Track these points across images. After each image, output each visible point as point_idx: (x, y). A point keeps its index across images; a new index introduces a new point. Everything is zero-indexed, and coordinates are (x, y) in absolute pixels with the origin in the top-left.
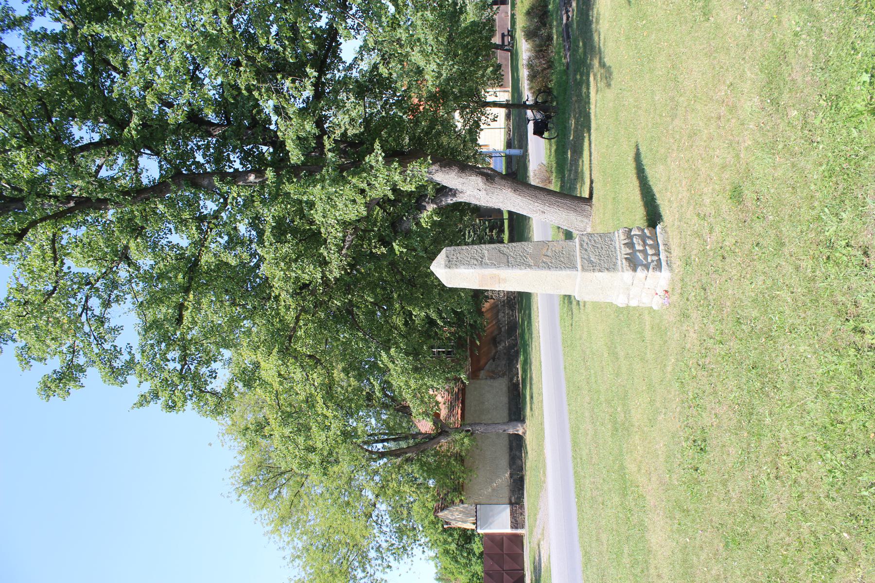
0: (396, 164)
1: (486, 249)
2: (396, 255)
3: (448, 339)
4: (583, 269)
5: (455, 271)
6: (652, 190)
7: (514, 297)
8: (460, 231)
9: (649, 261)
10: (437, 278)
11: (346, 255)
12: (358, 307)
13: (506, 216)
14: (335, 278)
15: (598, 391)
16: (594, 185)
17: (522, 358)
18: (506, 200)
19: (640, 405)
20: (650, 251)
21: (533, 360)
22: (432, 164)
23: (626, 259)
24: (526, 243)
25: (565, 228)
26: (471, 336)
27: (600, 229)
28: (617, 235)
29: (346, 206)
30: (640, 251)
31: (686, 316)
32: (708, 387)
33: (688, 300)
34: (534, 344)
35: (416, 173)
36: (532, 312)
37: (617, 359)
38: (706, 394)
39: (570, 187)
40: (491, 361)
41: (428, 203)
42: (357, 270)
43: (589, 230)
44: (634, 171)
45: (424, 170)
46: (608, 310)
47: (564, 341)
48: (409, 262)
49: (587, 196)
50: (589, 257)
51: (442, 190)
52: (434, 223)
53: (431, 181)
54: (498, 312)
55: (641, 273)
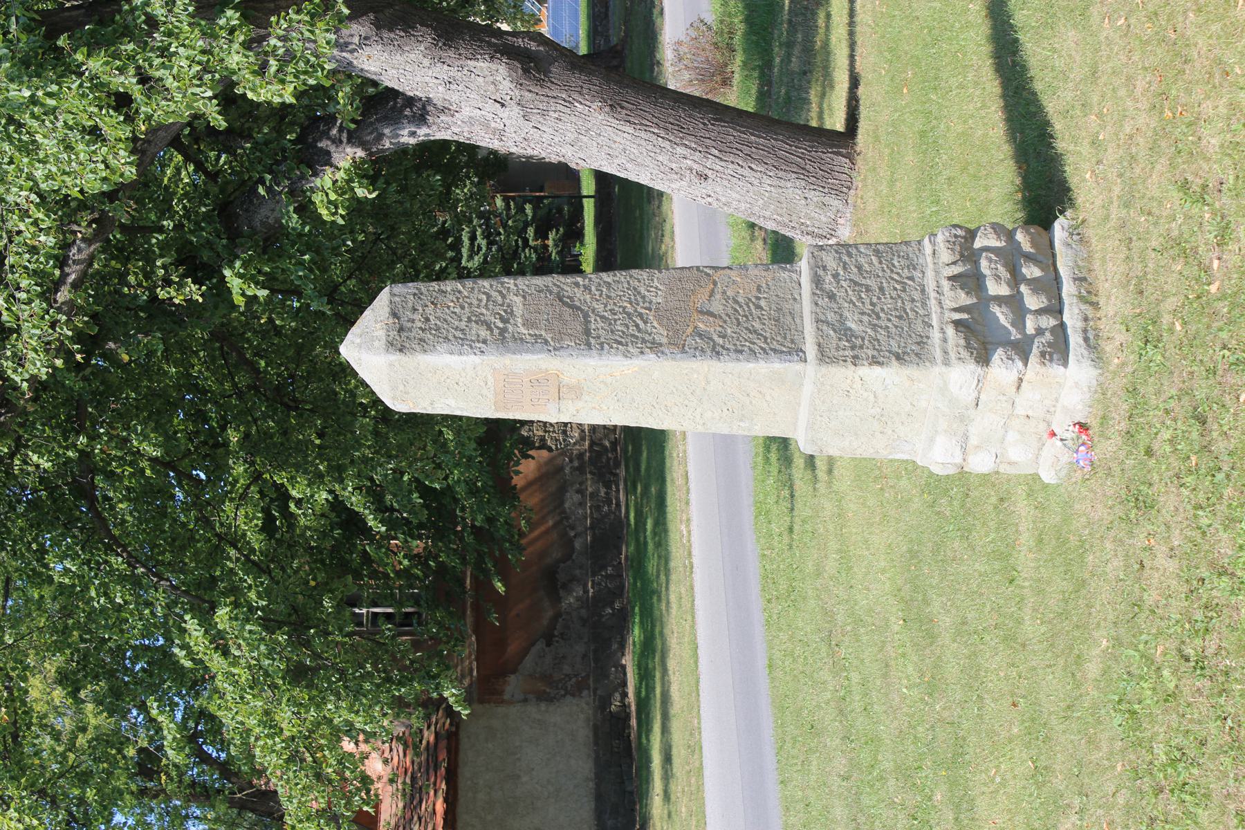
0: (232, 16)
1: (519, 293)
2: (234, 307)
3: (405, 573)
4: (824, 357)
5: (424, 363)
6: (1040, 108)
7: (614, 444)
8: (444, 233)
9: (1030, 327)
10: (363, 383)
11: (71, 304)
12: (110, 476)
13: (588, 187)
14: (33, 380)
15: (874, 740)
16: (861, 91)
17: (636, 633)
18: (587, 138)
19: (1004, 783)
20: (1033, 301)
21: (673, 642)
22: (350, 18)
23: (957, 324)
24: (643, 274)
25: (770, 226)
26: (479, 566)
27: (879, 231)
28: (928, 249)
29: (69, 148)
30: (999, 300)
31: (1143, 504)
32: (1213, 726)
33: (1149, 452)
34: (675, 592)
35: (297, 46)
36: (670, 489)
37: (932, 637)
38: (1209, 749)
39: (788, 99)
40: (540, 645)
41: (337, 142)
42: (110, 356)
43: (845, 233)
44: (986, 49)
45: (323, 36)
46: (904, 483)
47: (768, 579)
48: (278, 331)
49: (837, 122)
50: (842, 319)
51: (383, 104)
52: (357, 208)
53: (345, 72)
54: (562, 490)
55: (1002, 370)
